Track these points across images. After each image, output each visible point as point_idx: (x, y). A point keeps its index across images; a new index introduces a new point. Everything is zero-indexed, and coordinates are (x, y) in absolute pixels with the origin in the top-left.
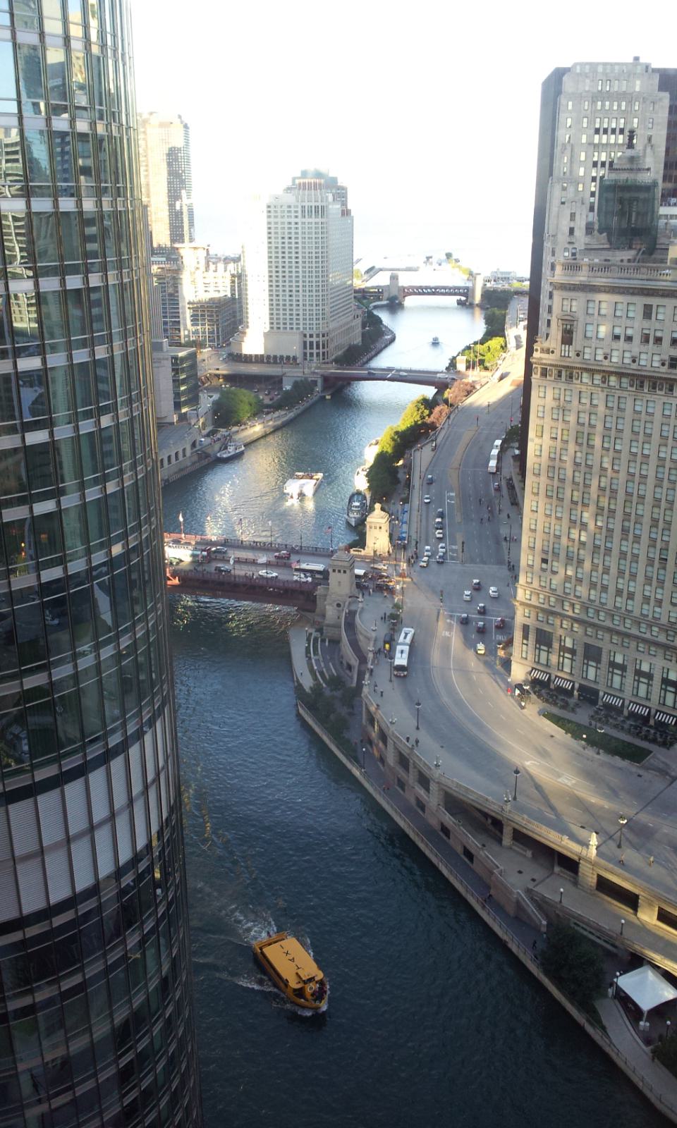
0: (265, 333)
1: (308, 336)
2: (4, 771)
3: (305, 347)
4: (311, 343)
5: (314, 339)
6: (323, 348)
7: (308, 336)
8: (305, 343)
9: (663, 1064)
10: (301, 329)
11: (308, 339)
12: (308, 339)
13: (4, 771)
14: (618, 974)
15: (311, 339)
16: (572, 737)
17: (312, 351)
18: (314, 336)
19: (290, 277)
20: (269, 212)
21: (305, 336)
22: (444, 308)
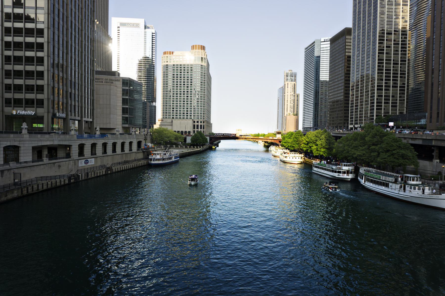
0: (155, 102)
1: (196, 122)
2: (35, 125)
3: (194, 128)
4: (198, 126)
5: (199, 124)
6: (204, 129)
7: (196, 122)
8: (194, 125)
9: (108, 32)
10: (192, 118)
11: (196, 124)
12: (196, 124)
13: (35, 125)
14: (423, 155)
15: (201, 124)
16: (30, 16)
17: (198, 124)
18: (199, 122)
19: (180, 84)
20: (174, 79)
21: (194, 122)
22: (145, 51)
